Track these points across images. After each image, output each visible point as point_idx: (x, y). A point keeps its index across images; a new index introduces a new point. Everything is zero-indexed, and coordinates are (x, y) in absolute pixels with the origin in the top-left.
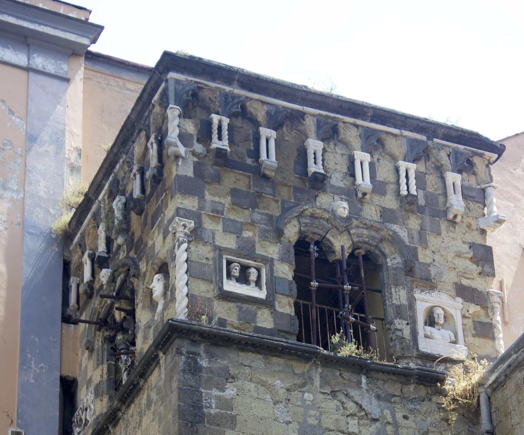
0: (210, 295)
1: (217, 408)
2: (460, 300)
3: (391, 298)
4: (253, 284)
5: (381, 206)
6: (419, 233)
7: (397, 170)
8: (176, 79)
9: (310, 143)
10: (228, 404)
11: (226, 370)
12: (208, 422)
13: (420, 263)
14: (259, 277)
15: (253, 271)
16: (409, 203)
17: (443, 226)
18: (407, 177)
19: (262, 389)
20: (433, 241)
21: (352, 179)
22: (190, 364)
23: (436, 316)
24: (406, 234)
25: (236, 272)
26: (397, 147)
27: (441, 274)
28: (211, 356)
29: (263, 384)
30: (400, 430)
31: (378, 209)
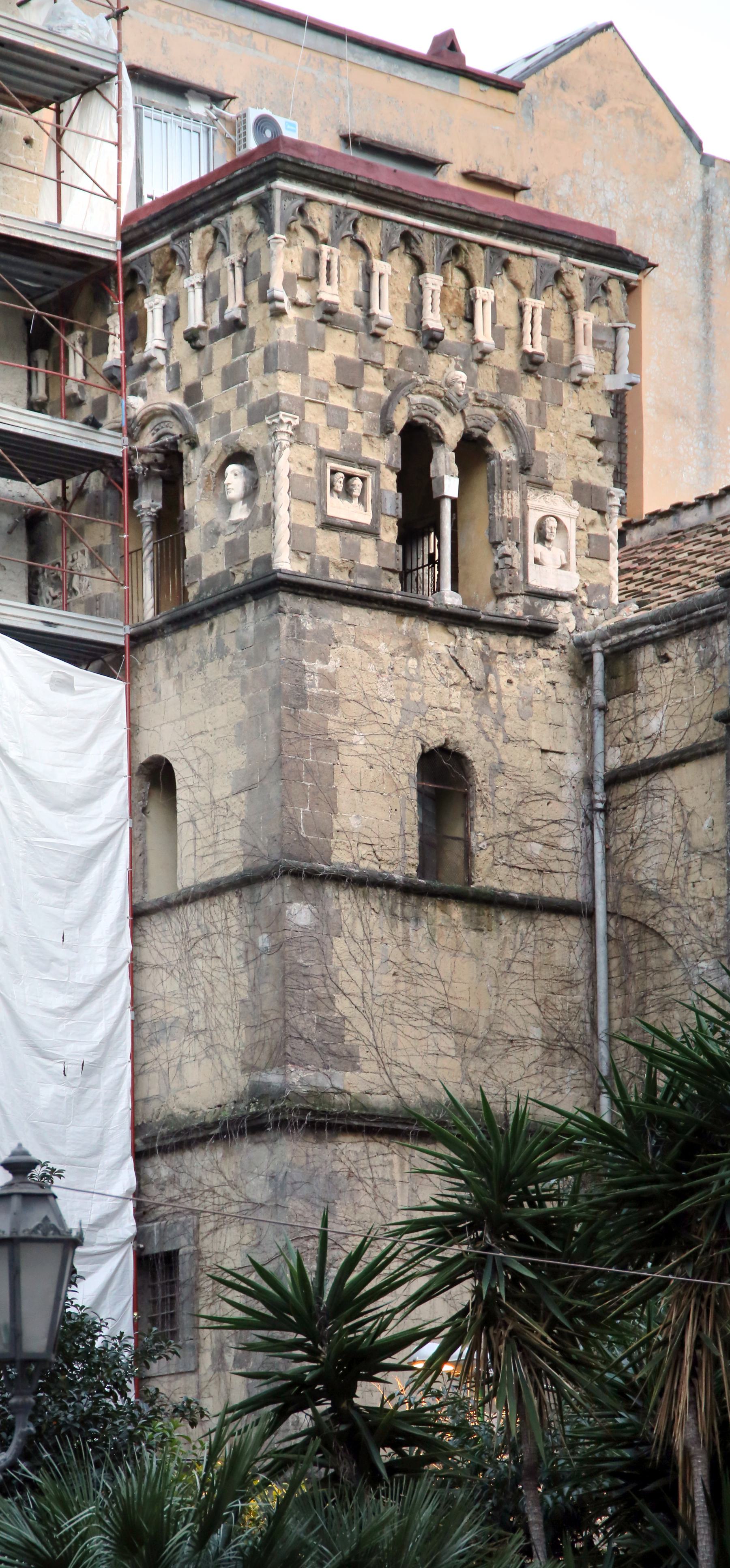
0: (313, 525)
1: (320, 687)
2: (576, 504)
3: (502, 507)
4: (356, 501)
5: (499, 368)
6: (539, 406)
7: (521, 309)
8: (594, 909)
9: (428, 280)
10: (329, 680)
11: (329, 631)
12: (311, 707)
13: (538, 453)
14: (364, 490)
15: (357, 482)
16: (532, 364)
17: (567, 390)
18: (532, 322)
19: (366, 655)
20: (553, 414)
21: (468, 325)
22: (293, 627)
23: (548, 530)
24: (523, 410)
25: (340, 487)
26: (524, 271)
27: (557, 467)
28: (314, 615)
29: (365, 648)
30: (503, 701)
31: (496, 371)
